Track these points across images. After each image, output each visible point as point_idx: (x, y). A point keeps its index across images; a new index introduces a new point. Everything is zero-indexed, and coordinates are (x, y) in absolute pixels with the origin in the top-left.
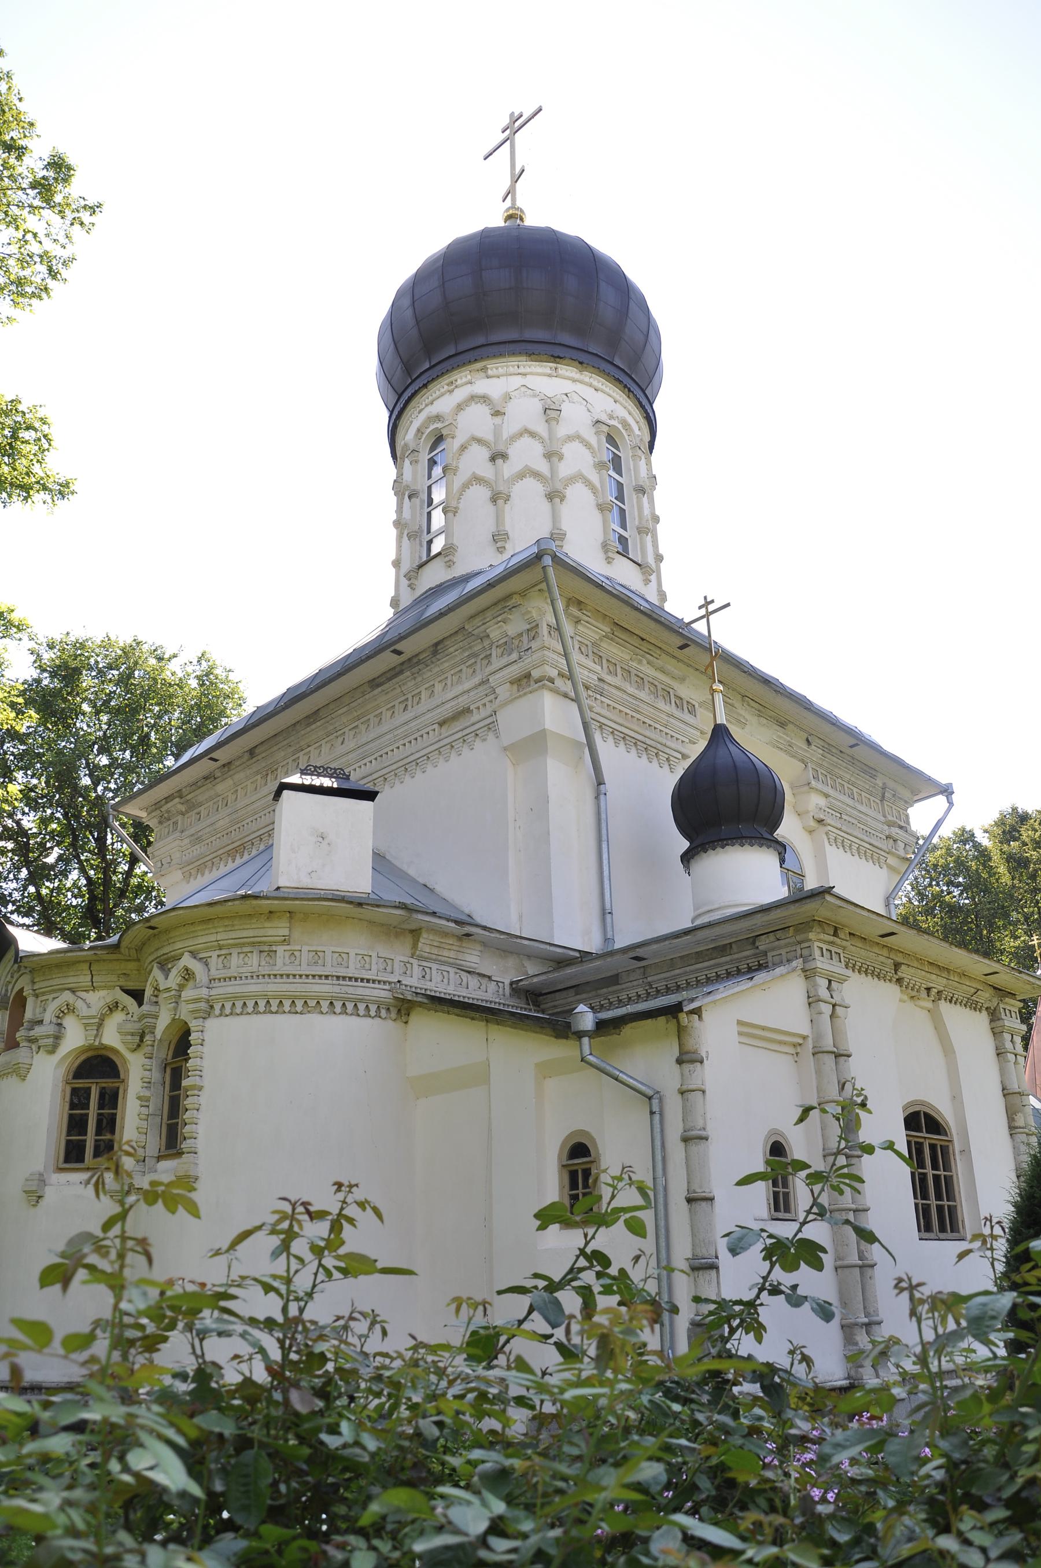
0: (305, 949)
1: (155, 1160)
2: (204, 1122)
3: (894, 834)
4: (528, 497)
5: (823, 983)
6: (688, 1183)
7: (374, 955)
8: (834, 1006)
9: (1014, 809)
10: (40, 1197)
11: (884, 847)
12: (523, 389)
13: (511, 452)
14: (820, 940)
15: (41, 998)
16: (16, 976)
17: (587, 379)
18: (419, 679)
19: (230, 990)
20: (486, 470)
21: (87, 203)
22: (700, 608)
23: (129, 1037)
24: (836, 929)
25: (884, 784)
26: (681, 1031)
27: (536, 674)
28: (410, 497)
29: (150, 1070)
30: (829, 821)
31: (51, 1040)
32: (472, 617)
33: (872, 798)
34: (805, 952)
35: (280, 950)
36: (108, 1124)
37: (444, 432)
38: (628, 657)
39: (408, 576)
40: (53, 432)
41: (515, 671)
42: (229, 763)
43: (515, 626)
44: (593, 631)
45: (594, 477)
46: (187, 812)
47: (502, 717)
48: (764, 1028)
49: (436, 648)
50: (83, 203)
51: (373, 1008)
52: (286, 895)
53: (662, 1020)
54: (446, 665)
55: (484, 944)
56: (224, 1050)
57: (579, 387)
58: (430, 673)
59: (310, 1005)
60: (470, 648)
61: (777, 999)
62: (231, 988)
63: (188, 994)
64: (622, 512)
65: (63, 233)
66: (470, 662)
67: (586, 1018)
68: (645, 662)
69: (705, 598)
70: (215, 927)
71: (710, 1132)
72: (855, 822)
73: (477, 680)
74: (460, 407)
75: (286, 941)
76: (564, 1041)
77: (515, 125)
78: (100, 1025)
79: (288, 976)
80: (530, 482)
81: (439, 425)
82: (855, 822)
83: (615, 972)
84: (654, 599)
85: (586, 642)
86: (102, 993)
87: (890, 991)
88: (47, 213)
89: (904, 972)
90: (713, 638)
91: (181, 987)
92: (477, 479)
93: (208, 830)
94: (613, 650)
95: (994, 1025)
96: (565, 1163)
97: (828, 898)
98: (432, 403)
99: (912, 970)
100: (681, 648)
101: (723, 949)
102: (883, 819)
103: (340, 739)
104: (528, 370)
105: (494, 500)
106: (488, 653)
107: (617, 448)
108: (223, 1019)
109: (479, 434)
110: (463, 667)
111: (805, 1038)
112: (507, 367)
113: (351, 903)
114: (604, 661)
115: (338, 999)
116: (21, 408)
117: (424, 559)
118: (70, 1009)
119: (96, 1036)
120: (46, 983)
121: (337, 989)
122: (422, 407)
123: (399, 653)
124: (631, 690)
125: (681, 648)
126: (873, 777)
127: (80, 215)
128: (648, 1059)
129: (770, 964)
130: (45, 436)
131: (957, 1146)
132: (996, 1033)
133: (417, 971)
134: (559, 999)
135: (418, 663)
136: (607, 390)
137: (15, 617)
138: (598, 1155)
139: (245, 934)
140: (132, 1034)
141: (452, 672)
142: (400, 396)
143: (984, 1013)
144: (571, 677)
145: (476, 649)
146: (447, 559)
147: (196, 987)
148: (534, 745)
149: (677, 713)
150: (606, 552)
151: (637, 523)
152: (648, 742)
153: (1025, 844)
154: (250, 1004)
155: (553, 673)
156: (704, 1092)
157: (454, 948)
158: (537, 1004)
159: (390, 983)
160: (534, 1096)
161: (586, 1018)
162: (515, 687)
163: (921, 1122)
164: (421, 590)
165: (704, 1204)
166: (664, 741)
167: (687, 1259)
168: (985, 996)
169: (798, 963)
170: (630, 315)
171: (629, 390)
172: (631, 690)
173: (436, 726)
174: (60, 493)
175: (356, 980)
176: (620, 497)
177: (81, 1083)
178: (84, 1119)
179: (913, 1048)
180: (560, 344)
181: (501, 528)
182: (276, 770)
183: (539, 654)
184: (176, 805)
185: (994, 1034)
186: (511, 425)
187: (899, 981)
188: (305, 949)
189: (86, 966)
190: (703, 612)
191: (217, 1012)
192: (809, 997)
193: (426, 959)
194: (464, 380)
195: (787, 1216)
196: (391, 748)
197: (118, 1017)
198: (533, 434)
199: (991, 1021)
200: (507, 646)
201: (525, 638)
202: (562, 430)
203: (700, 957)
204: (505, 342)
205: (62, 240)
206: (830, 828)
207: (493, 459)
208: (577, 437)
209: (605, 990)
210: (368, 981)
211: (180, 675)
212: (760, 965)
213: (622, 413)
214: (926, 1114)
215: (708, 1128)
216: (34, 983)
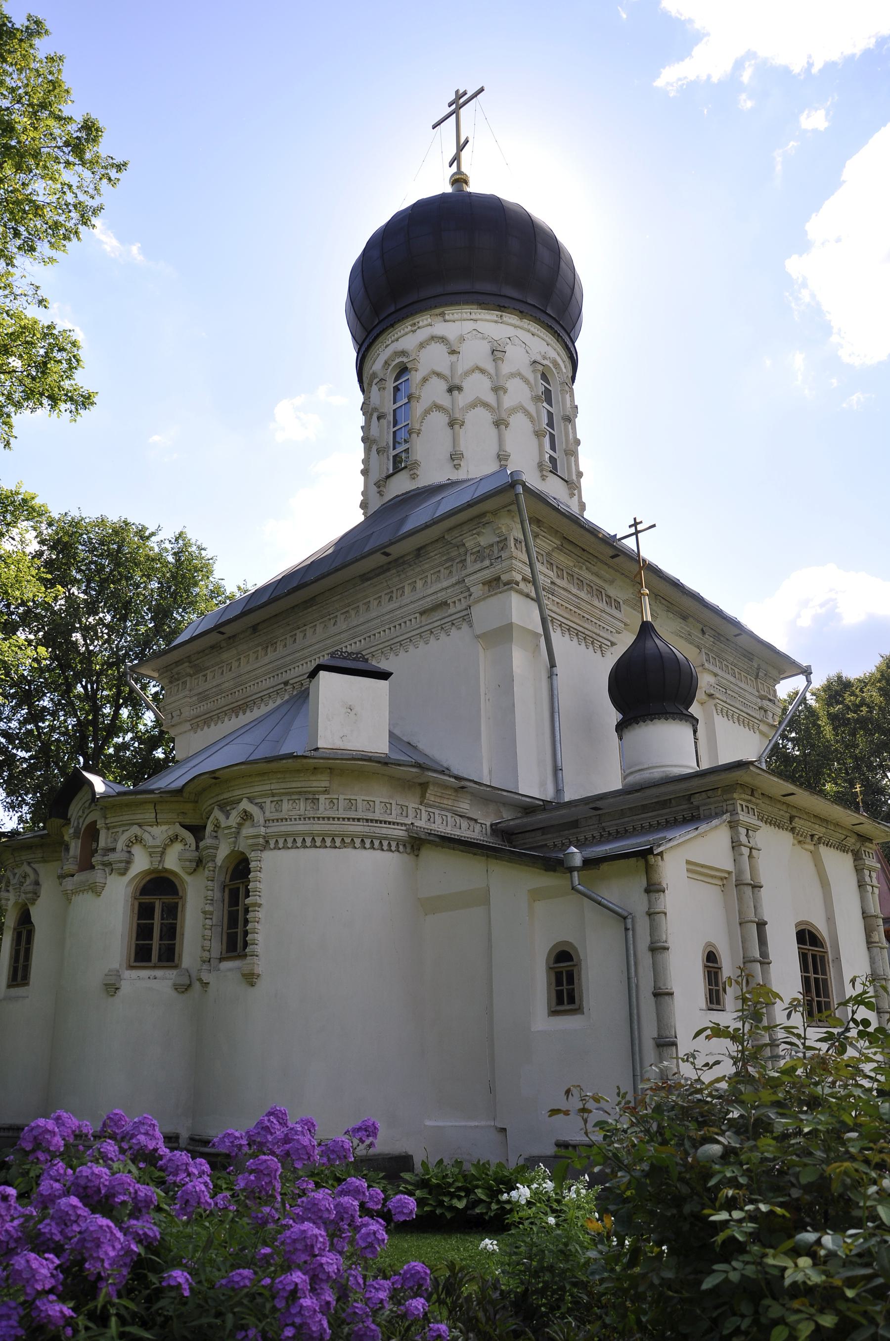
0: (342, 797)
1: (218, 961)
2: (263, 933)
3: (765, 706)
4: (478, 423)
5: (743, 831)
6: (655, 982)
7: (394, 803)
8: (751, 849)
9: (840, 678)
10: (117, 989)
11: (758, 717)
12: (474, 332)
13: (465, 385)
14: (741, 799)
15: (111, 831)
16: (87, 812)
17: (526, 326)
18: (403, 576)
19: (283, 829)
20: (444, 400)
21: (114, 161)
22: (630, 526)
23: (188, 863)
24: (753, 791)
25: (759, 665)
26: (649, 870)
27: (505, 578)
28: (379, 418)
29: (212, 890)
30: (718, 695)
31: (124, 864)
32: (451, 529)
33: (749, 677)
34: (730, 808)
35: (322, 798)
36: (171, 932)
37: (409, 366)
38: (572, 564)
39: (378, 485)
40: (82, 354)
41: (487, 574)
42: (234, 636)
43: (486, 538)
44: (544, 544)
45: (531, 408)
46: (195, 674)
47: (477, 611)
48: (702, 866)
49: (420, 552)
50: (111, 161)
51: (394, 844)
52: (325, 755)
53: (633, 861)
54: (427, 566)
55: (472, 794)
56: (279, 875)
57: (520, 333)
58: (412, 572)
59: (347, 841)
60: (448, 553)
61: (710, 844)
62: (284, 828)
63: (247, 831)
64: (552, 437)
65: (92, 186)
66: (447, 565)
67: (576, 855)
68: (584, 568)
69: (635, 519)
70: (269, 780)
71: (669, 944)
72: (737, 696)
73: (454, 580)
74: (422, 346)
75: (326, 792)
76: (552, 873)
77: (459, 102)
78: (163, 853)
79: (329, 818)
80: (480, 411)
81: (405, 360)
82: (737, 696)
83: (576, 818)
84: (575, 509)
85: (542, 552)
86: (164, 828)
87: (785, 838)
88: (79, 168)
89: (797, 823)
90: (642, 554)
91: (240, 825)
92: (438, 407)
93: (214, 690)
94: (561, 559)
95: (857, 863)
96: (552, 966)
97: (752, 768)
98: (397, 340)
99: (802, 822)
100: (613, 557)
101: (664, 804)
102: (757, 694)
103: (332, 621)
104: (479, 317)
105: (451, 424)
106: (463, 558)
107: (548, 383)
108: (276, 852)
109: (438, 369)
110: (441, 568)
111: (729, 873)
112: (461, 313)
113: (379, 762)
114: (555, 568)
115: (367, 837)
116: (55, 332)
117: (391, 471)
118: (138, 840)
119: (160, 862)
120: (117, 819)
121: (367, 829)
122: (388, 343)
123: (387, 554)
124: (574, 591)
125: (613, 557)
126: (751, 660)
127: (109, 171)
128: (621, 891)
129: (702, 816)
130: (74, 356)
131: (831, 956)
132: (859, 870)
133: (425, 816)
134: (532, 837)
135: (404, 563)
136: (541, 335)
137: (37, 502)
138: (580, 960)
139: (294, 785)
140: (190, 861)
141: (432, 572)
142: (369, 333)
143: (850, 854)
144: (534, 582)
145: (452, 554)
146: (412, 472)
147: (253, 826)
148: (503, 634)
149: (608, 609)
150: (541, 471)
151: (564, 447)
152: (587, 632)
153: (848, 708)
154: (299, 841)
155: (519, 578)
156: (665, 914)
157: (452, 797)
158: (510, 842)
159: (405, 825)
160: (527, 916)
161: (576, 855)
162: (486, 588)
163: (807, 938)
164: (388, 496)
165: (667, 997)
166: (598, 632)
167: (654, 1039)
168: (851, 841)
169: (727, 817)
170: (560, 273)
171: (559, 335)
172: (574, 591)
173: (417, 615)
174: (83, 404)
175: (381, 822)
176: (551, 424)
177: (147, 899)
178: (150, 928)
179: (803, 882)
180: (505, 296)
181: (457, 449)
182: (276, 643)
183: (507, 562)
184: (185, 668)
185: (857, 870)
186: (465, 362)
187: (793, 830)
188: (342, 797)
189: (151, 806)
190: (633, 530)
191: (272, 846)
192: (733, 842)
193: (431, 806)
194: (425, 322)
195: (718, 1007)
196: (378, 631)
197: (178, 847)
198: (482, 371)
199: (855, 860)
200: (480, 555)
201: (495, 548)
202: (506, 368)
203: (645, 808)
204: (461, 293)
205: (92, 192)
206: (718, 701)
207: (450, 390)
208: (518, 375)
209: (567, 832)
210: (390, 823)
211: (157, 550)
212: (693, 816)
213: (552, 354)
214: (810, 932)
215: (669, 941)
216: (106, 818)
